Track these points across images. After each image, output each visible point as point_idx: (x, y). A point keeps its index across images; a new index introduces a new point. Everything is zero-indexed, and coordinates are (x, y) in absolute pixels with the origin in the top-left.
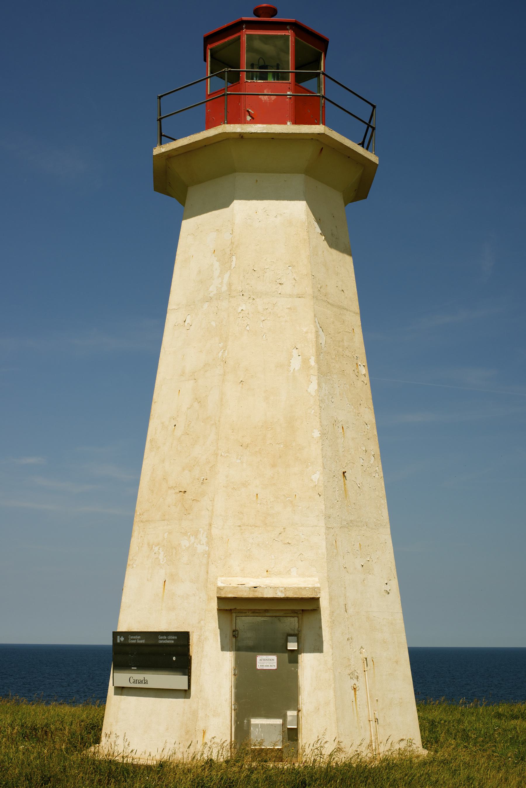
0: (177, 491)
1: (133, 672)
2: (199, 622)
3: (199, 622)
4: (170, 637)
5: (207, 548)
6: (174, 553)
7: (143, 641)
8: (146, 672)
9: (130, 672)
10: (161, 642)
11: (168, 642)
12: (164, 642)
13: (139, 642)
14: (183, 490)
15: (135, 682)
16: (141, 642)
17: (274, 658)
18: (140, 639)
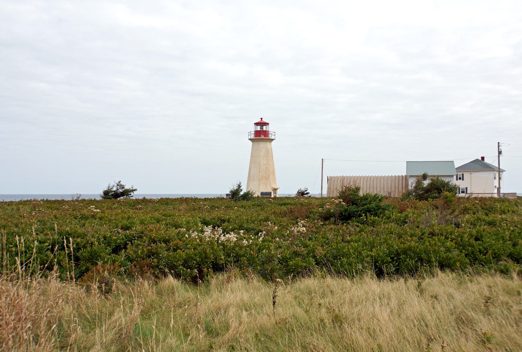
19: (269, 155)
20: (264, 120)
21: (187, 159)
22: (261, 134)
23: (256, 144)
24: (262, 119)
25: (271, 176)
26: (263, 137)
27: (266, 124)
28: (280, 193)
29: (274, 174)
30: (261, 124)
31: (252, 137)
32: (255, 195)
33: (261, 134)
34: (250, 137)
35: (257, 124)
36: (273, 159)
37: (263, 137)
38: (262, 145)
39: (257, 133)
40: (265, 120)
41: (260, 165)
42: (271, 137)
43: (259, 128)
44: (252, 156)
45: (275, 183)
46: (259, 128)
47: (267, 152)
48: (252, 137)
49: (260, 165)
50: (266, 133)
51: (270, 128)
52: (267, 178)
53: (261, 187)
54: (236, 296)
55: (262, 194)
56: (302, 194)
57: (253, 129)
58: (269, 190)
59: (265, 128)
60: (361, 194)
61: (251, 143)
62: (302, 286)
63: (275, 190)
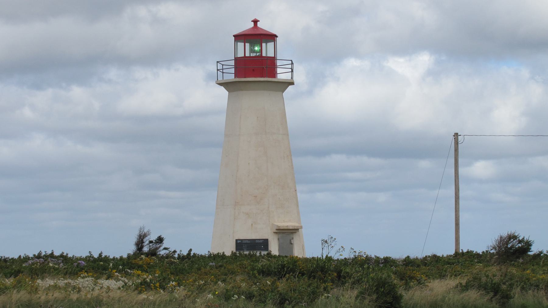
21: (78, 250)
24: (255, 22)
27: (272, 37)
30: (256, 36)
31: (230, 77)
32: (228, 253)
35: (238, 38)
38: (256, 101)
42: (282, 74)
48: (230, 77)
51: (282, 51)
54: (85, 282)
55: (240, 244)
56: (408, 257)
57: (230, 51)
59: (268, 50)
60: (474, 252)
61: (223, 92)
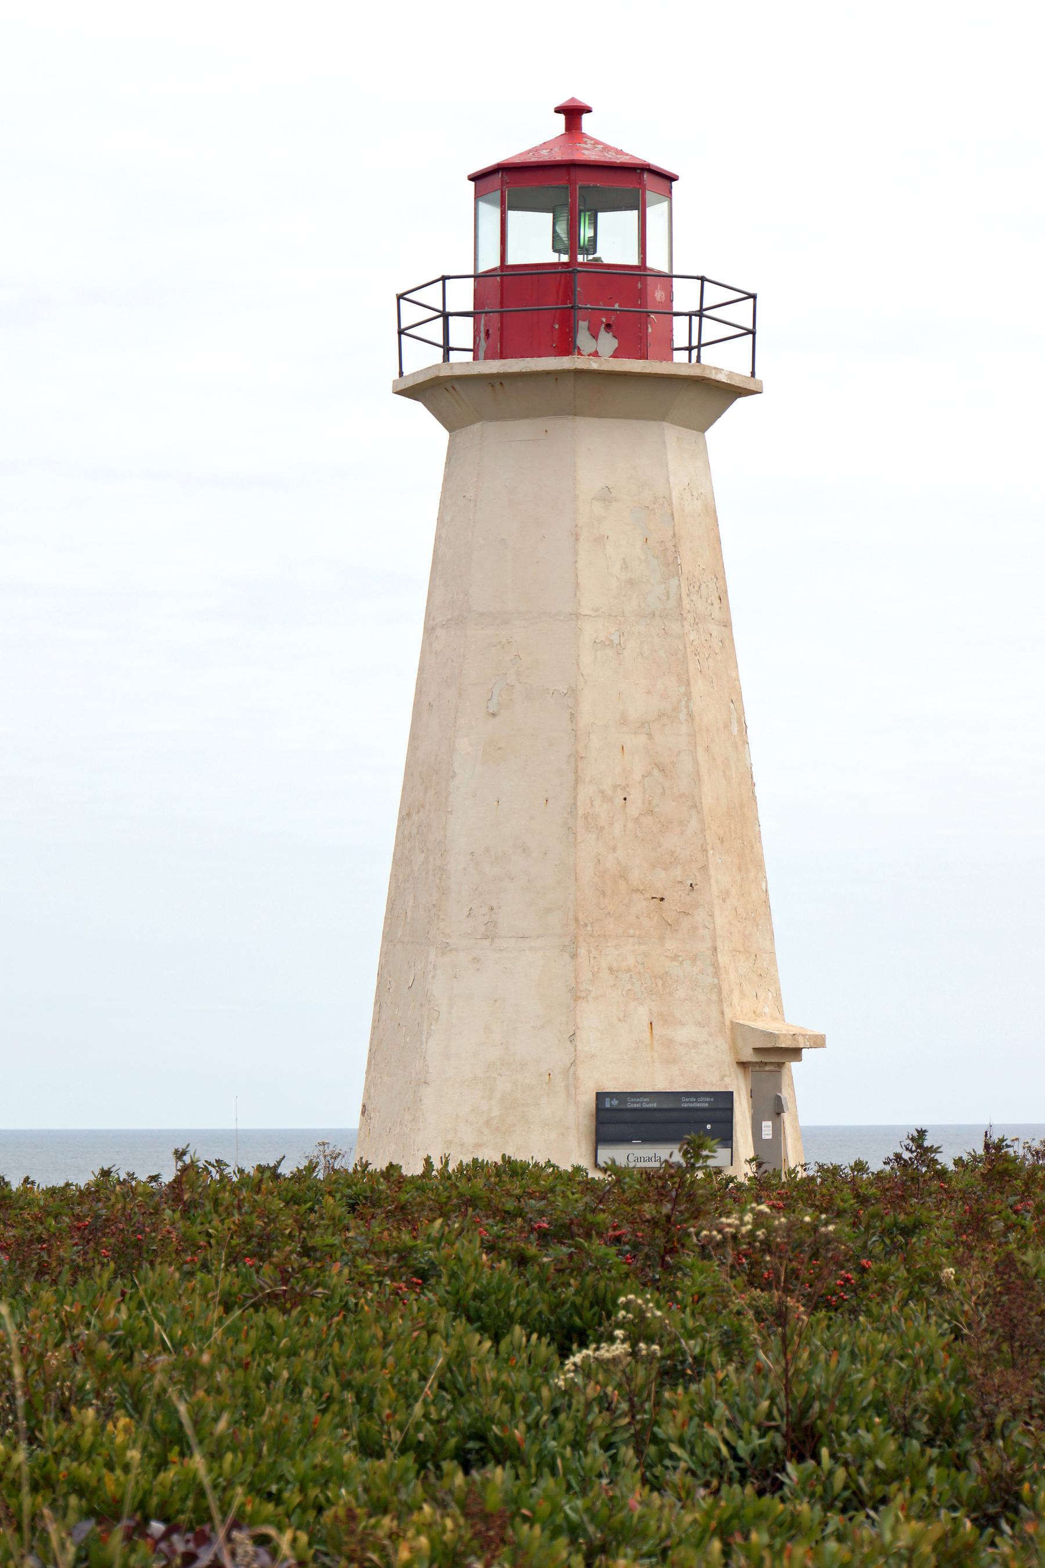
0: (648, 895)
1: (635, 1147)
2: (722, 1079)
3: (722, 1079)
4: (702, 1099)
5: (716, 980)
6: (660, 985)
7: (655, 1105)
8: (659, 1146)
9: (629, 1146)
10: (686, 1105)
11: (698, 1105)
12: (691, 1105)
13: (645, 1106)
14: (659, 896)
15: (637, 1160)
16: (650, 1106)
17: (580, 322)
18: (647, 1103)
19: (683, 593)
20: (611, 133)
22: (569, 318)
23: (512, 447)
25: (721, 876)
26: (598, 352)
27: (633, 182)
28: (844, 1110)
29: (748, 857)
33: (569, 318)
34: (422, 359)
35: (509, 183)
36: (727, 644)
37: (598, 352)
38: (601, 460)
39: (522, 308)
40: (615, 132)
41: (561, 753)
43: (533, 239)
44: (449, 612)
45: (765, 975)
46: (534, 238)
47: (669, 558)
49: (561, 753)
50: (632, 301)
51: (682, 241)
52: (672, 908)
53: (591, 1019)
57: (455, 241)
58: (701, 1066)
59: (614, 238)
61: (424, 431)
62: (651, 1542)
63: (770, 1060)
